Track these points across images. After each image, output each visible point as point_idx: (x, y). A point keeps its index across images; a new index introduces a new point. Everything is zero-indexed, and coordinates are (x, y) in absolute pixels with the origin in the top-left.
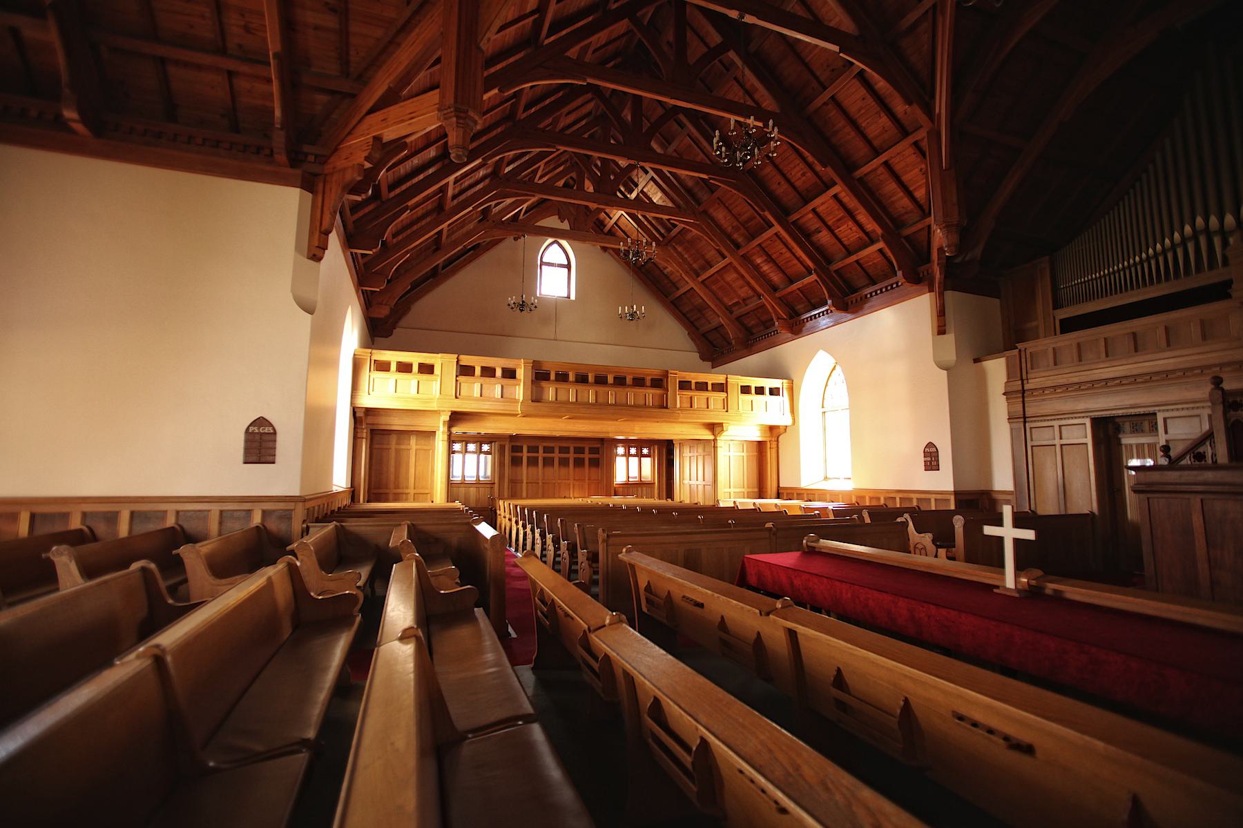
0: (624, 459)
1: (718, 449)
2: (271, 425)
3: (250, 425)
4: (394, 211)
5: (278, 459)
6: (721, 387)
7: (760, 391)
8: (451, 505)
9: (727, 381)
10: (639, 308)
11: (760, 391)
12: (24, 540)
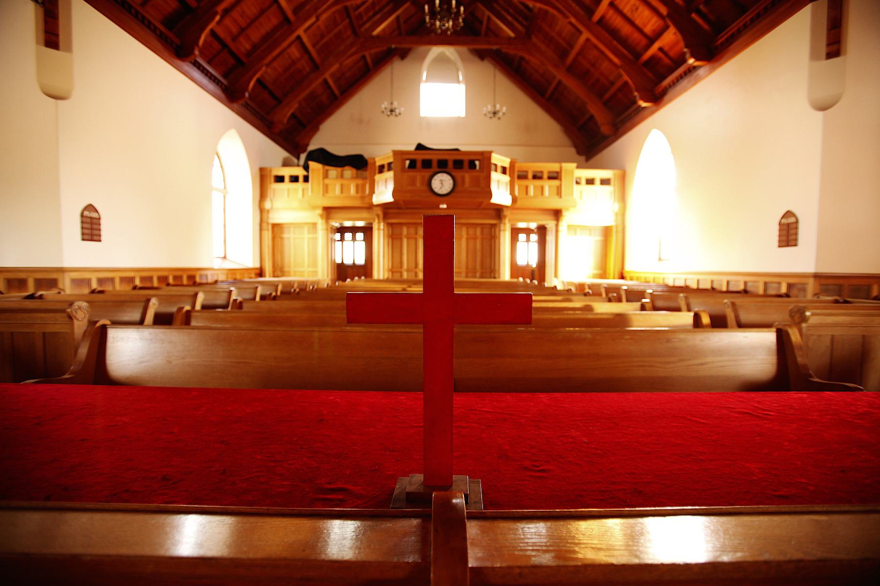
2: (96, 211)
3: (782, 218)
4: (601, 46)
5: (103, 238)
6: (555, 176)
7: (590, 182)
8: (515, 280)
10: (501, 107)
11: (590, 182)
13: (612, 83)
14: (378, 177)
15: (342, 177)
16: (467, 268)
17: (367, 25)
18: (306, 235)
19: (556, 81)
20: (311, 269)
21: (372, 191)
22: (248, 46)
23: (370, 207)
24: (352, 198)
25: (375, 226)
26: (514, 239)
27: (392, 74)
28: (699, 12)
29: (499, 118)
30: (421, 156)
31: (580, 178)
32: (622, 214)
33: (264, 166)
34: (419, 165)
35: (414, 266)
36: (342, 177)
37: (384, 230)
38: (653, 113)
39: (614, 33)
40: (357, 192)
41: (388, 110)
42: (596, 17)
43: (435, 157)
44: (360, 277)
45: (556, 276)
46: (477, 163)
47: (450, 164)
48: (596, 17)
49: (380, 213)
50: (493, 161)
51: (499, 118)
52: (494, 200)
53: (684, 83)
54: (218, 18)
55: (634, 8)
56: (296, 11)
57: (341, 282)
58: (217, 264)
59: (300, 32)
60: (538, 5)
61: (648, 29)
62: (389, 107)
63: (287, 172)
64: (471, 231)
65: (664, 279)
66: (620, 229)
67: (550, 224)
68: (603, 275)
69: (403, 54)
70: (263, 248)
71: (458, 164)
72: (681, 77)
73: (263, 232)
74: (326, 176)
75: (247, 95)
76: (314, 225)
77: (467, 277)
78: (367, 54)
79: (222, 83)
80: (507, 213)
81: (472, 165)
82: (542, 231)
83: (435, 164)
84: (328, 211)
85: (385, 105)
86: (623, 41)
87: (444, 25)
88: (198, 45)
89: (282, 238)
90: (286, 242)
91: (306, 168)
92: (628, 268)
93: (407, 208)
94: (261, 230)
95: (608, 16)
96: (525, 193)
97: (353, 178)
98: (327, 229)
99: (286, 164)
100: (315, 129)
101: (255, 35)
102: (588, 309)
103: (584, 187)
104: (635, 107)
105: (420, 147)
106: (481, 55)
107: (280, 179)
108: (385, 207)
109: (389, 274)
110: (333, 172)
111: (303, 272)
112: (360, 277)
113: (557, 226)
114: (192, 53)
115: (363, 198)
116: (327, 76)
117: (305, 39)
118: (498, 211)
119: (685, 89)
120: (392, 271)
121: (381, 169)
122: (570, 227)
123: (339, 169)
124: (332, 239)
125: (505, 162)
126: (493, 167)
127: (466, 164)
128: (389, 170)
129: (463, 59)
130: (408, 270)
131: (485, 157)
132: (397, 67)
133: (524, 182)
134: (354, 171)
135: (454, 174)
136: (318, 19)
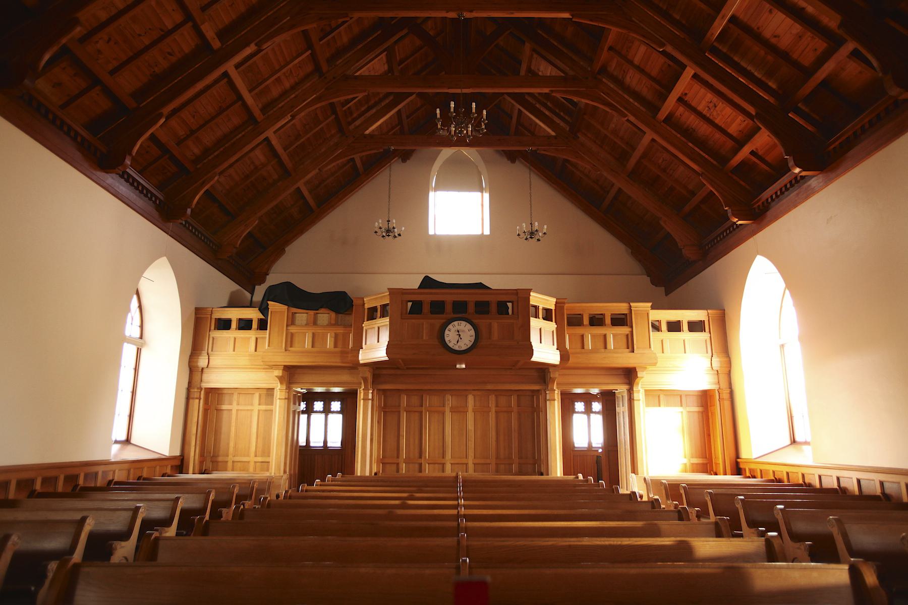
0: (585, 417)
1: (635, 402)
6: (621, 320)
7: (674, 327)
9: (631, 310)
10: (541, 225)
12: (367, 477)
13: (693, 194)
14: (366, 324)
15: (315, 323)
16: (497, 458)
17: (358, 122)
18: (256, 407)
19: (613, 192)
20: (259, 459)
21: (359, 346)
22: (197, 151)
23: (355, 366)
24: (329, 353)
25: (361, 395)
26: (567, 412)
27: (390, 171)
28: (798, 112)
29: (539, 240)
30: (429, 296)
31: (660, 322)
32: (727, 373)
33: (201, 305)
34: (426, 308)
35: (417, 455)
36: (315, 323)
37: (373, 400)
38: (754, 233)
39: (688, 133)
40: (336, 346)
41: (383, 230)
42: (662, 115)
43: (449, 297)
44: (334, 475)
45: (634, 471)
46: (510, 305)
47: (471, 308)
48: (662, 115)
49: (369, 375)
50: (533, 301)
51: (539, 240)
52: (535, 358)
53: (792, 195)
54: (162, 120)
55: (711, 105)
56: (264, 109)
57: (306, 487)
58: (115, 453)
59: (270, 133)
60: (584, 101)
61: (733, 129)
62: (385, 226)
63: (234, 314)
64: (503, 400)
65: (803, 475)
66: (726, 395)
67: (621, 389)
68: (707, 467)
69: (405, 156)
70: (189, 422)
71: (483, 308)
72: (785, 189)
73: (191, 401)
74: (291, 322)
75: (189, 211)
76: (270, 391)
77: (497, 471)
78: (357, 158)
79: (157, 198)
80: (554, 374)
81: (502, 308)
82: (609, 400)
83: (449, 308)
84: (291, 373)
85: (380, 223)
86: (702, 143)
87: (461, 132)
88: (130, 154)
89: (219, 411)
90: (225, 415)
91: (264, 309)
92: (745, 454)
93: (407, 368)
94: (188, 398)
95: (678, 113)
96: (579, 345)
97: (330, 325)
98: (288, 399)
99: (233, 303)
100: (279, 251)
101: (208, 137)
102: (683, 552)
103: (665, 335)
104: (727, 224)
105: (428, 283)
106: (512, 157)
107: (224, 325)
108: (376, 366)
109: (378, 467)
110: (302, 316)
111: (249, 462)
112: (334, 475)
113: (630, 392)
114: (121, 162)
115: (344, 353)
116: (301, 184)
117: (275, 142)
118: (543, 370)
119: (795, 205)
120: (383, 461)
121: (372, 314)
122: (648, 393)
123: (312, 312)
124: (294, 412)
125: (549, 302)
126: (532, 310)
127: (493, 308)
128: (383, 316)
129: (487, 161)
130: (408, 461)
131: (523, 296)
132: (397, 170)
133: (579, 330)
134: (333, 315)
135: (475, 321)
136: (293, 117)
